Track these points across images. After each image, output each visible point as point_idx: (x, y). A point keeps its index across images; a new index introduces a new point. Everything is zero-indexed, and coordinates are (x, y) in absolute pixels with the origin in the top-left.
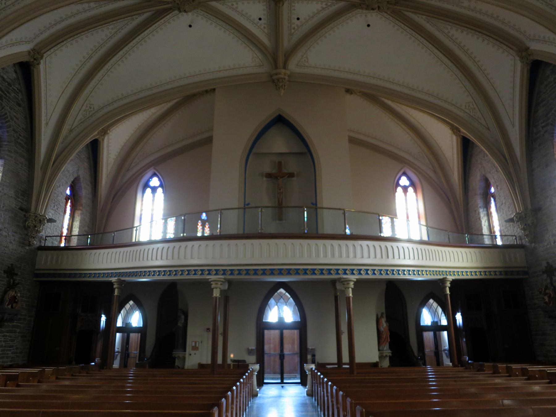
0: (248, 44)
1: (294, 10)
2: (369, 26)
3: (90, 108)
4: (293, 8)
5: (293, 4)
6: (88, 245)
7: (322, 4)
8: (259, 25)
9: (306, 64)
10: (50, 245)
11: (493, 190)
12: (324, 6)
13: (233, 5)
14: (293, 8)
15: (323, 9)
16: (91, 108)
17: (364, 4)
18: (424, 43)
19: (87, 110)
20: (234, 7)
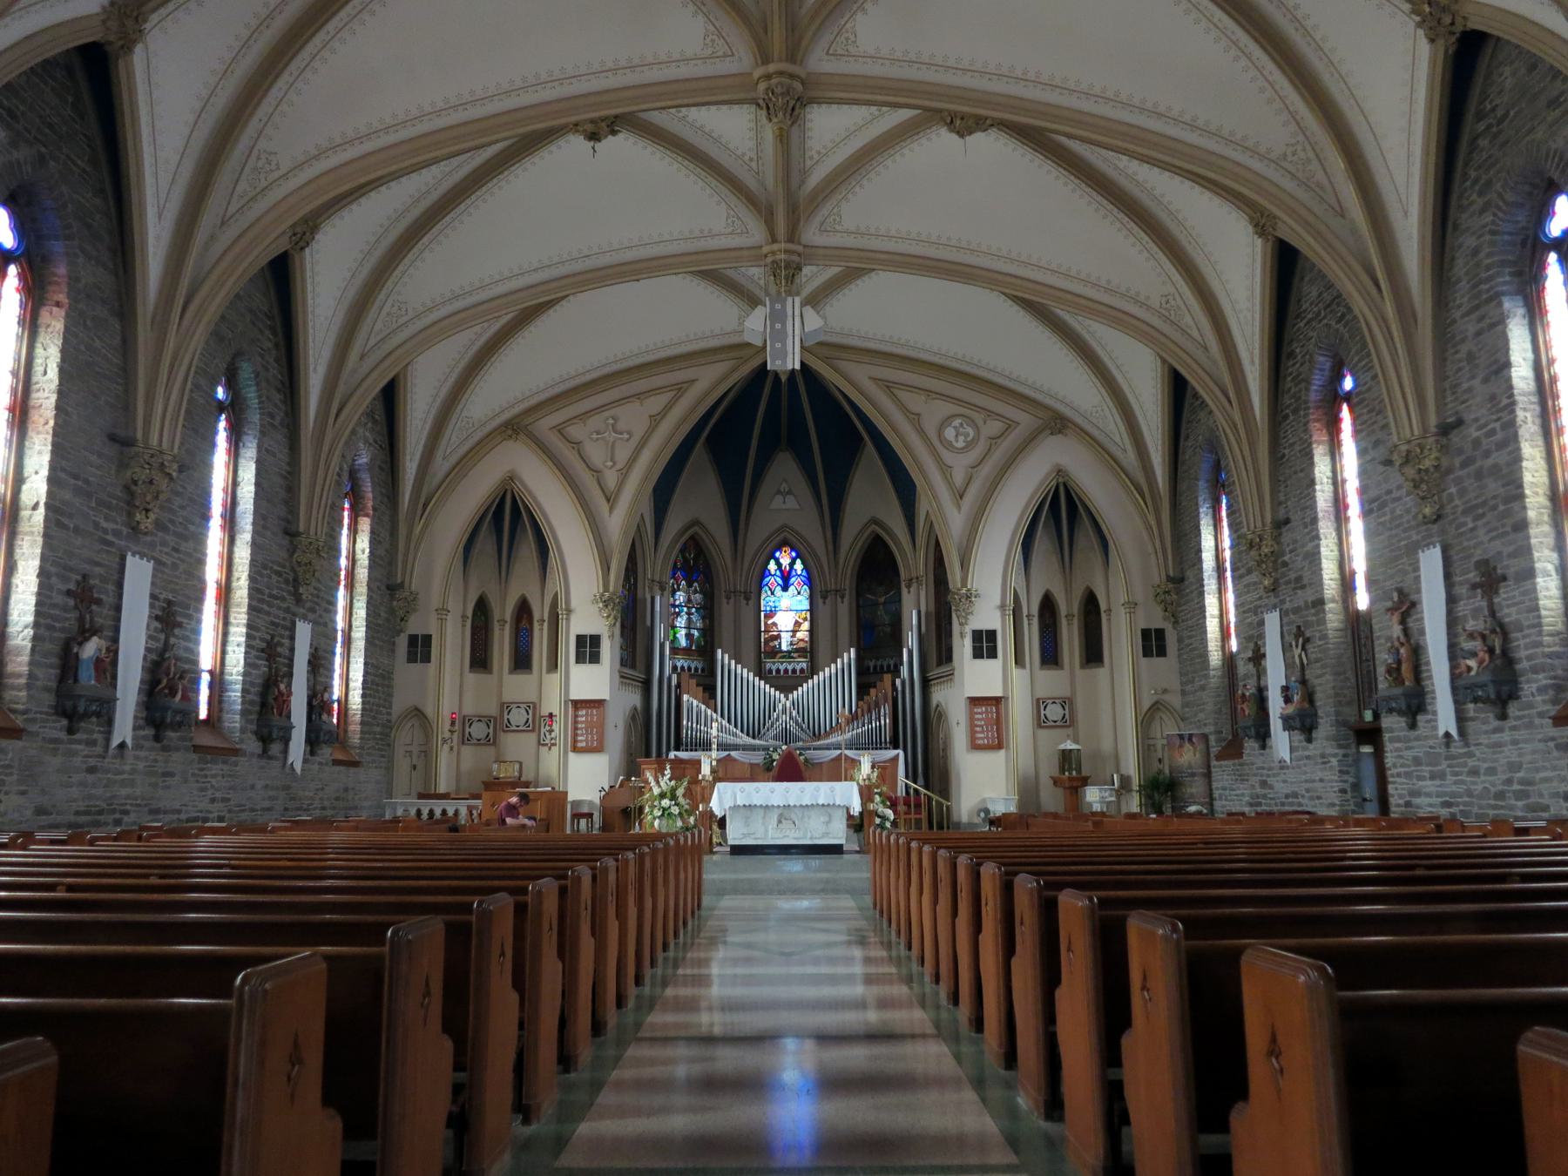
9: (837, 227)
11: (1348, 383)
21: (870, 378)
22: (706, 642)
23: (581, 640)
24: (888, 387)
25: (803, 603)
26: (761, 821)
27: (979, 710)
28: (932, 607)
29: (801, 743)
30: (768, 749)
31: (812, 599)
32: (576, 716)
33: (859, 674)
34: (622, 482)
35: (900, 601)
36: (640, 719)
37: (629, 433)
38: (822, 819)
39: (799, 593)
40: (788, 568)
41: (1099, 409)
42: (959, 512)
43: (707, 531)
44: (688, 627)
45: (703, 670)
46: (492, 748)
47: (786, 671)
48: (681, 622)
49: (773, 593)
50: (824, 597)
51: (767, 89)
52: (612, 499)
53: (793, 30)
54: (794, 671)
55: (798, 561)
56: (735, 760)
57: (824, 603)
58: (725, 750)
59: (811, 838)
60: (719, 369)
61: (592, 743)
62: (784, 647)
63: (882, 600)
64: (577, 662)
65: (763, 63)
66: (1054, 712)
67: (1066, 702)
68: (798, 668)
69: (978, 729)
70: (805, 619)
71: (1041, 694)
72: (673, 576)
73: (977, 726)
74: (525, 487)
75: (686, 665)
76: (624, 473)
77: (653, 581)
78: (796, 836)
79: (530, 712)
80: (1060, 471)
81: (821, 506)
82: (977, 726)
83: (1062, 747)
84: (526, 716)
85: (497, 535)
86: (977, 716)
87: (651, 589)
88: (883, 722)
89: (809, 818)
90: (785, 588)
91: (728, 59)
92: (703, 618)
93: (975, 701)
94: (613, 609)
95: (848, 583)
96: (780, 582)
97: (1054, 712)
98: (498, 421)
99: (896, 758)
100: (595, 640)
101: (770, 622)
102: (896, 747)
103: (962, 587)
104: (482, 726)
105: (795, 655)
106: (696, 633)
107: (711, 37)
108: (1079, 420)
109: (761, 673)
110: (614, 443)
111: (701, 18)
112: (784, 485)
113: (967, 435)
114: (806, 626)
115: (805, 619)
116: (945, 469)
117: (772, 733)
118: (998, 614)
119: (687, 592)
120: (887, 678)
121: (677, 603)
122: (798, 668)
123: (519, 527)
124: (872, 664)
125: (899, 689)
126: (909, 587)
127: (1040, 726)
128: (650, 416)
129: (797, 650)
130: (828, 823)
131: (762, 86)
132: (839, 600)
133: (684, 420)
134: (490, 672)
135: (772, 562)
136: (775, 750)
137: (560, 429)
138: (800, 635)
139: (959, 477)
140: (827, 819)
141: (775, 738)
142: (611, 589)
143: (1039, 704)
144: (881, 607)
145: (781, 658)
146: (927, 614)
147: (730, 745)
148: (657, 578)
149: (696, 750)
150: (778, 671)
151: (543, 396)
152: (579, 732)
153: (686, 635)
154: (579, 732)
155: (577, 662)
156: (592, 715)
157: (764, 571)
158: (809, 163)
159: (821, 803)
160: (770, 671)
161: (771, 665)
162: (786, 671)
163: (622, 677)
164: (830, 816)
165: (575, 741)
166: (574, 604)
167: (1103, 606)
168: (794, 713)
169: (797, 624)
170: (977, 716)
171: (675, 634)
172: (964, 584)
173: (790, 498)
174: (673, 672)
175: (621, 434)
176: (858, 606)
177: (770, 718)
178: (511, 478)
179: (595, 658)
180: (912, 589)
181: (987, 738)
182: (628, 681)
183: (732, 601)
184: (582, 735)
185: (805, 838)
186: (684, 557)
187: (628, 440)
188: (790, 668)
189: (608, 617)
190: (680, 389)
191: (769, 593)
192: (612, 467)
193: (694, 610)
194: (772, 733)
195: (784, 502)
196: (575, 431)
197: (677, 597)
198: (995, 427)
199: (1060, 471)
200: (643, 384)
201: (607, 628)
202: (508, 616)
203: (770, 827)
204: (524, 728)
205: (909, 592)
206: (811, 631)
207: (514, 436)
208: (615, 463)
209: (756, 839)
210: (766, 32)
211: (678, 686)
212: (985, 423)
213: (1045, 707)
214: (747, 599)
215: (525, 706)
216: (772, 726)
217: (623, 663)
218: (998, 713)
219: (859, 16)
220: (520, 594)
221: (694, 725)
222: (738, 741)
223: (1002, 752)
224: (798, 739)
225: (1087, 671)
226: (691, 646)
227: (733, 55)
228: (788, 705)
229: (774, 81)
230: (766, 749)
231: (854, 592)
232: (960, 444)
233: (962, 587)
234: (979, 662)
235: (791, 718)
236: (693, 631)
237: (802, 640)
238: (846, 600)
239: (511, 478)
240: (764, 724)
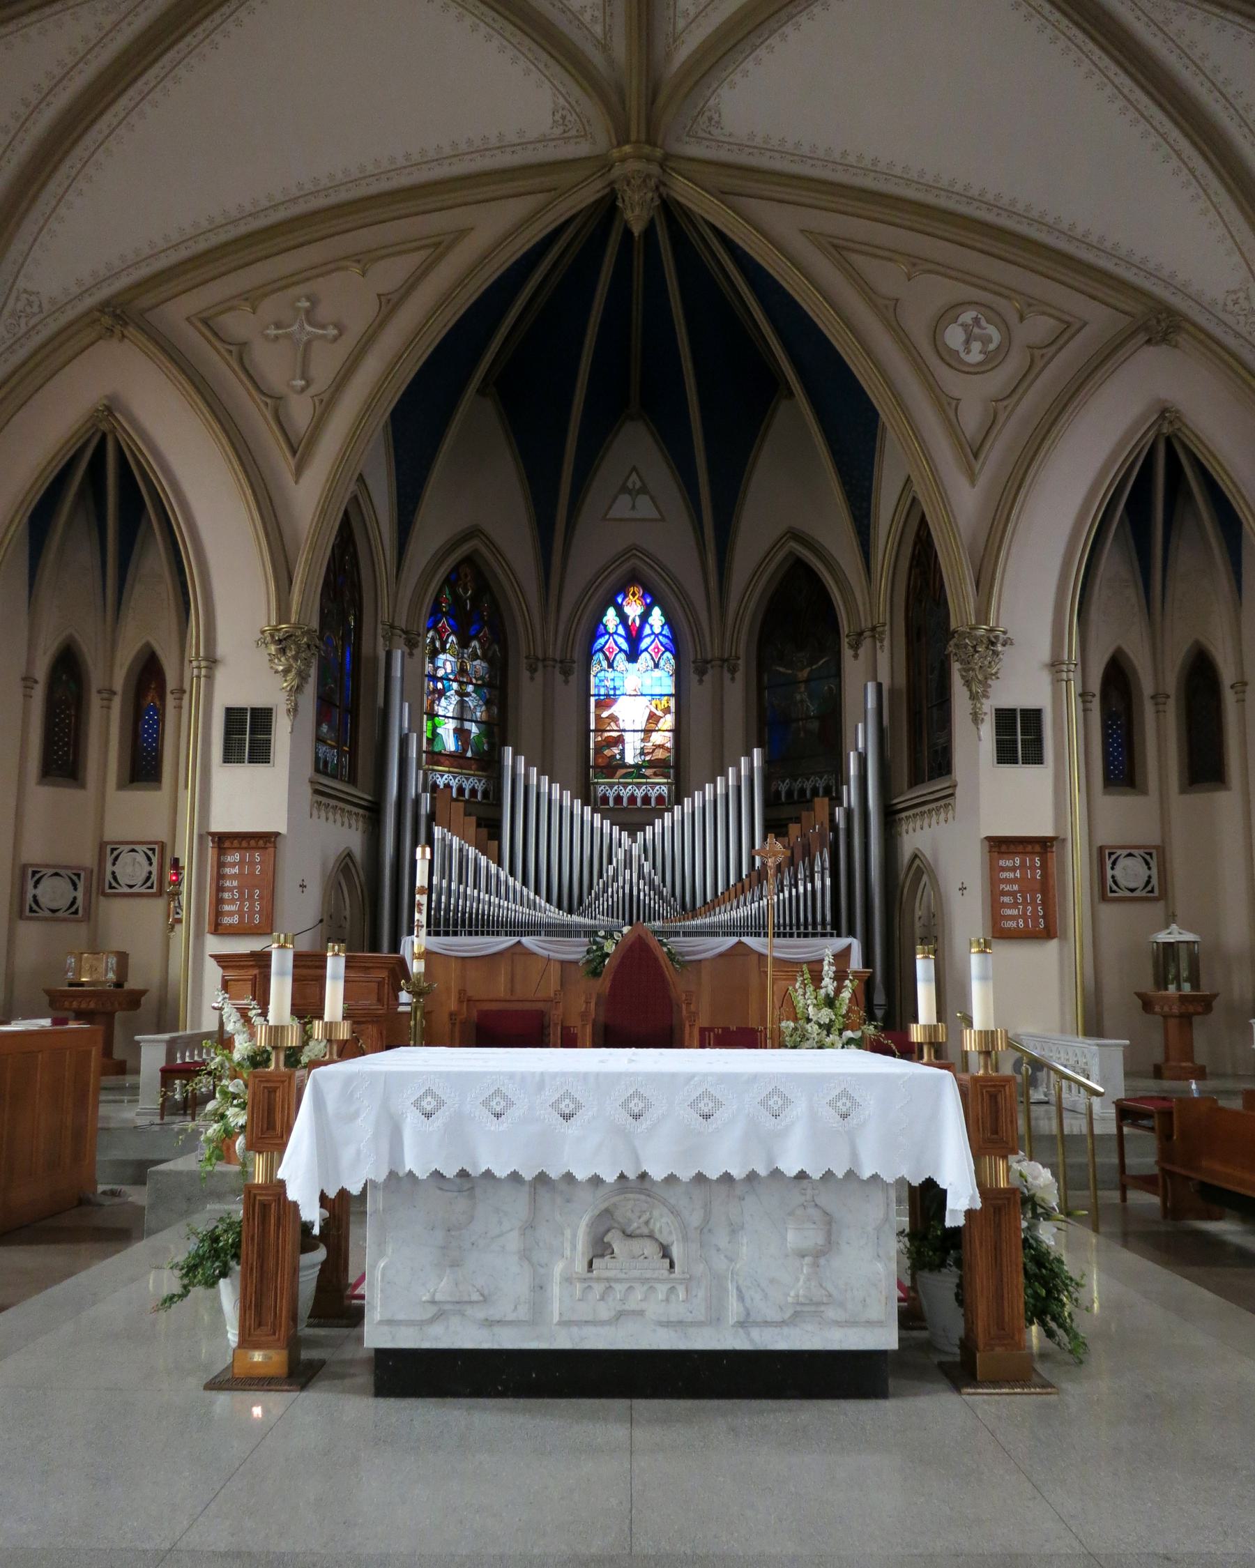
3: (30, 304)
6: (783, 799)
10: (1064, 1116)
16: (31, 307)
18: (985, 206)
19: (21, 311)
21: (802, 231)
22: (491, 745)
23: (234, 717)
24: (835, 247)
25: (663, 682)
26: (513, 1242)
27: (1009, 863)
28: (902, 681)
29: (658, 924)
30: (596, 933)
31: (678, 675)
32: (221, 865)
33: (768, 804)
34: (323, 414)
35: (838, 674)
36: (360, 877)
37: (338, 326)
38: (793, 1238)
39: (656, 666)
40: (638, 623)
41: (1241, 295)
42: (973, 483)
43: (491, 544)
44: (460, 718)
45: (486, 794)
46: (83, 926)
47: (632, 799)
48: (447, 707)
49: (611, 665)
50: (701, 672)
52: (300, 450)
54: (646, 799)
55: (657, 612)
56: (530, 954)
57: (701, 681)
58: (514, 934)
59: (742, 1325)
60: (515, 210)
61: (251, 918)
62: (630, 759)
63: (804, 674)
64: (227, 760)
66: (1130, 872)
67: (1155, 855)
68: (653, 794)
69: (1006, 899)
70: (667, 711)
71: (1106, 837)
72: (434, 626)
73: (1004, 893)
74: (133, 421)
75: (454, 783)
76: (326, 406)
77: (392, 627)
78: (677, 1310)
79: (155, 860)
80: (1165, 413)
81: (702, 528)
82: (1004, 893)
83: (1163, 937)
84: (147, 868)
86: (1004, 875)
87: (389, 639)
88: (818, 884)
89: (735, 1229)
90: (633, 656)
92: (488, 703)
93: (1000, 846)
94: (295, 658)
95: (743, 646)
96: (625, 646)
97: (1130, 872)
98: (89, 302)
99: (848, 948)
100: (262, 718)
101: (605, 715)
102: (851, 933)
103: (979, 622)
104: (63, 885)
105: (648, 772)
106: (474, 729)
108: (1201, 319)
109: (586, 795)
110: (308, 344)
112: (634, 476)
113: (986, 340)
114: (668, 722)
115: (667, 711)
116: (946, 406)
117: (603, 903)
118: (1045, 678)
119: (459, 656)
120: (821, 803)
121: (440, 673)
122: (653, 794)
123: (143, 527)
124: (783, 788)
125: (842, 825)
126: (855, 646)
127: (1104, 898)
128: (379, 295)
129: (652, 764)
130: (820, 1254)
132: (727, 676)
133: (446, 299)
134: (82, 786)
135: (611, 612)
136: (609, 935)
137: (206, 322)
138: (657, 738)
139: (971, 420)
140: (814, 1238)
141: (610, 912)
142: (293, 619)
143: (1103, 857)
144: (802, 687)
145: (624, 776)
146: (892, 691)
147: (522, 924)
148: (402, 622)
149: (455, 934)
150: (618, 799)
151: (174, 258)
152: (226, 895)
153: (456, 730)
154: (226, 895)
155: (227, 760)
156: (252, 863)
157: (597, 627)
159: (790, 1168)
160: (605, 799)
161: (605, 788)
162: (632, 799)
163: (317, 792)
164: (829, 1222)
165: (218, 914)
166: (224, 647)
167: (1227, 675)
168: (647, 867)
169: (653, 718)
170: (1004, 875)
171: (435, 728)
172: (983, 615)
173: (643, 500)
174: (425, 790)
175: (323, 327)
176: (760, 689)
177: (601, 876)
178: (110, 408)
179: (261, 754)
180: (861, 651)
181: (1024, 916)
182: (333, 802)
183: (539, 675)
184: (232, 901)
185: (715, 1319)
186: (454, 593)
187: (335, 339)
188: (639, 793)
189: (286, 671)
190: (439, 248)
191: (605, 664)
192: (303, 390)
193: (470, 688)
194: (603, 903)
195: (633, 507)
196: (238, 324)
197: (440, 663)
198: (1040, 327)
199: (1165, 413)
200: (364, 238)
201: (285, 695)
202: (118, 683)
203: (559, 1268)
204: (143, 890)
205: (856, 656)
206: (677, 731)
207: (118, 329)
208: (309, 383)
209: (489, 1323)
211: (432, 818)
212: (1022, 318)
213: (1114, 863)
214: (566, 673)
215: (144, 848)
216: (605, 891)
217: (321, 767)
218: (1044, 867)
220: (144, 641)
221: (453, 886)
222: (521, 913)
223: (1053, 945)
224: (653, 916)
225: (1198, 799)
226: (465, 751)
228: (635, 852)
230: (591, 932)
231: (754, 664)
232: (975, 356)
233: (979, 622)
234: (1008, 769)
235: (641, 875)
236: (467, 725)
237: (661, 746)
238: (739, 675)
239: (110, 408)
240: (591, 887)
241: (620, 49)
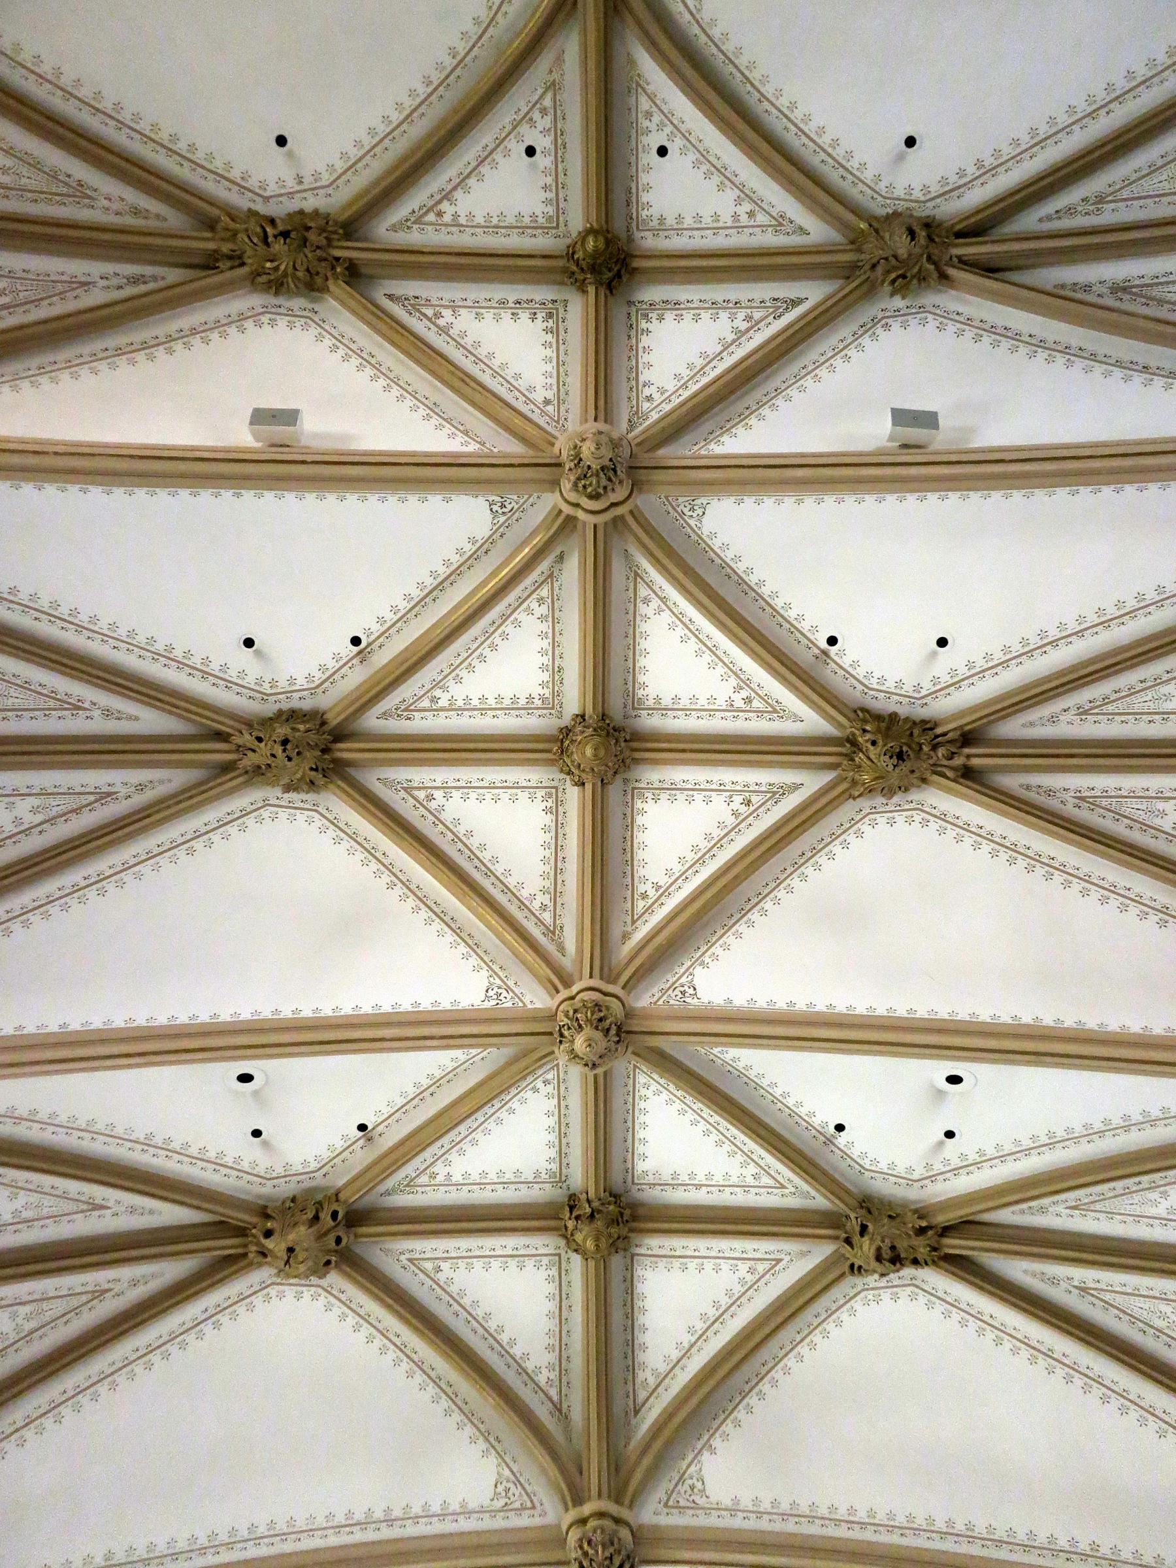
0: (714, 50)
1: (545, 188)
2: (281, 141)
4: (549, 381)
5: (551, 210)
7: (456, 216)
8: (669, 129)
12: (447, 313)
13: (751, 214)
14: (549, 381)
15: (447, 196)
17: (318, 247)
20: (747, 206)
51: (581, 1540)
53: (617, 1470)
65: (574, 1506)
85: (202, 735)
91: (527, 1512)
107: (504, 1483)
111: (493, 1460)
131: (573, 1537)
158: (642, 1395)
210: (581, 1473)
219: (706, 1455)
227: (534, 1507)
229: (592, 1524)
241: (577, 1405)
